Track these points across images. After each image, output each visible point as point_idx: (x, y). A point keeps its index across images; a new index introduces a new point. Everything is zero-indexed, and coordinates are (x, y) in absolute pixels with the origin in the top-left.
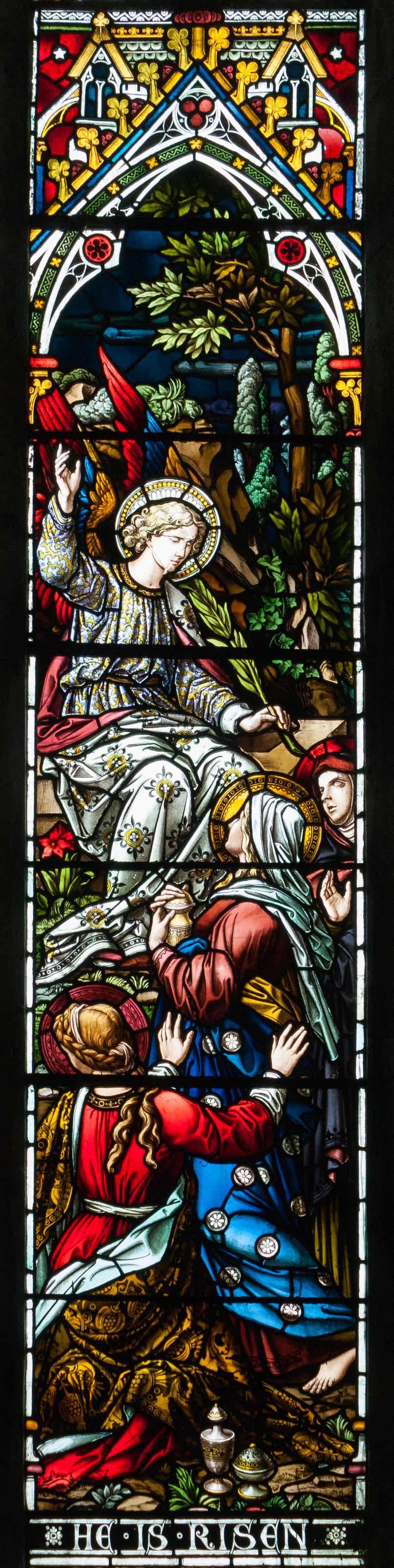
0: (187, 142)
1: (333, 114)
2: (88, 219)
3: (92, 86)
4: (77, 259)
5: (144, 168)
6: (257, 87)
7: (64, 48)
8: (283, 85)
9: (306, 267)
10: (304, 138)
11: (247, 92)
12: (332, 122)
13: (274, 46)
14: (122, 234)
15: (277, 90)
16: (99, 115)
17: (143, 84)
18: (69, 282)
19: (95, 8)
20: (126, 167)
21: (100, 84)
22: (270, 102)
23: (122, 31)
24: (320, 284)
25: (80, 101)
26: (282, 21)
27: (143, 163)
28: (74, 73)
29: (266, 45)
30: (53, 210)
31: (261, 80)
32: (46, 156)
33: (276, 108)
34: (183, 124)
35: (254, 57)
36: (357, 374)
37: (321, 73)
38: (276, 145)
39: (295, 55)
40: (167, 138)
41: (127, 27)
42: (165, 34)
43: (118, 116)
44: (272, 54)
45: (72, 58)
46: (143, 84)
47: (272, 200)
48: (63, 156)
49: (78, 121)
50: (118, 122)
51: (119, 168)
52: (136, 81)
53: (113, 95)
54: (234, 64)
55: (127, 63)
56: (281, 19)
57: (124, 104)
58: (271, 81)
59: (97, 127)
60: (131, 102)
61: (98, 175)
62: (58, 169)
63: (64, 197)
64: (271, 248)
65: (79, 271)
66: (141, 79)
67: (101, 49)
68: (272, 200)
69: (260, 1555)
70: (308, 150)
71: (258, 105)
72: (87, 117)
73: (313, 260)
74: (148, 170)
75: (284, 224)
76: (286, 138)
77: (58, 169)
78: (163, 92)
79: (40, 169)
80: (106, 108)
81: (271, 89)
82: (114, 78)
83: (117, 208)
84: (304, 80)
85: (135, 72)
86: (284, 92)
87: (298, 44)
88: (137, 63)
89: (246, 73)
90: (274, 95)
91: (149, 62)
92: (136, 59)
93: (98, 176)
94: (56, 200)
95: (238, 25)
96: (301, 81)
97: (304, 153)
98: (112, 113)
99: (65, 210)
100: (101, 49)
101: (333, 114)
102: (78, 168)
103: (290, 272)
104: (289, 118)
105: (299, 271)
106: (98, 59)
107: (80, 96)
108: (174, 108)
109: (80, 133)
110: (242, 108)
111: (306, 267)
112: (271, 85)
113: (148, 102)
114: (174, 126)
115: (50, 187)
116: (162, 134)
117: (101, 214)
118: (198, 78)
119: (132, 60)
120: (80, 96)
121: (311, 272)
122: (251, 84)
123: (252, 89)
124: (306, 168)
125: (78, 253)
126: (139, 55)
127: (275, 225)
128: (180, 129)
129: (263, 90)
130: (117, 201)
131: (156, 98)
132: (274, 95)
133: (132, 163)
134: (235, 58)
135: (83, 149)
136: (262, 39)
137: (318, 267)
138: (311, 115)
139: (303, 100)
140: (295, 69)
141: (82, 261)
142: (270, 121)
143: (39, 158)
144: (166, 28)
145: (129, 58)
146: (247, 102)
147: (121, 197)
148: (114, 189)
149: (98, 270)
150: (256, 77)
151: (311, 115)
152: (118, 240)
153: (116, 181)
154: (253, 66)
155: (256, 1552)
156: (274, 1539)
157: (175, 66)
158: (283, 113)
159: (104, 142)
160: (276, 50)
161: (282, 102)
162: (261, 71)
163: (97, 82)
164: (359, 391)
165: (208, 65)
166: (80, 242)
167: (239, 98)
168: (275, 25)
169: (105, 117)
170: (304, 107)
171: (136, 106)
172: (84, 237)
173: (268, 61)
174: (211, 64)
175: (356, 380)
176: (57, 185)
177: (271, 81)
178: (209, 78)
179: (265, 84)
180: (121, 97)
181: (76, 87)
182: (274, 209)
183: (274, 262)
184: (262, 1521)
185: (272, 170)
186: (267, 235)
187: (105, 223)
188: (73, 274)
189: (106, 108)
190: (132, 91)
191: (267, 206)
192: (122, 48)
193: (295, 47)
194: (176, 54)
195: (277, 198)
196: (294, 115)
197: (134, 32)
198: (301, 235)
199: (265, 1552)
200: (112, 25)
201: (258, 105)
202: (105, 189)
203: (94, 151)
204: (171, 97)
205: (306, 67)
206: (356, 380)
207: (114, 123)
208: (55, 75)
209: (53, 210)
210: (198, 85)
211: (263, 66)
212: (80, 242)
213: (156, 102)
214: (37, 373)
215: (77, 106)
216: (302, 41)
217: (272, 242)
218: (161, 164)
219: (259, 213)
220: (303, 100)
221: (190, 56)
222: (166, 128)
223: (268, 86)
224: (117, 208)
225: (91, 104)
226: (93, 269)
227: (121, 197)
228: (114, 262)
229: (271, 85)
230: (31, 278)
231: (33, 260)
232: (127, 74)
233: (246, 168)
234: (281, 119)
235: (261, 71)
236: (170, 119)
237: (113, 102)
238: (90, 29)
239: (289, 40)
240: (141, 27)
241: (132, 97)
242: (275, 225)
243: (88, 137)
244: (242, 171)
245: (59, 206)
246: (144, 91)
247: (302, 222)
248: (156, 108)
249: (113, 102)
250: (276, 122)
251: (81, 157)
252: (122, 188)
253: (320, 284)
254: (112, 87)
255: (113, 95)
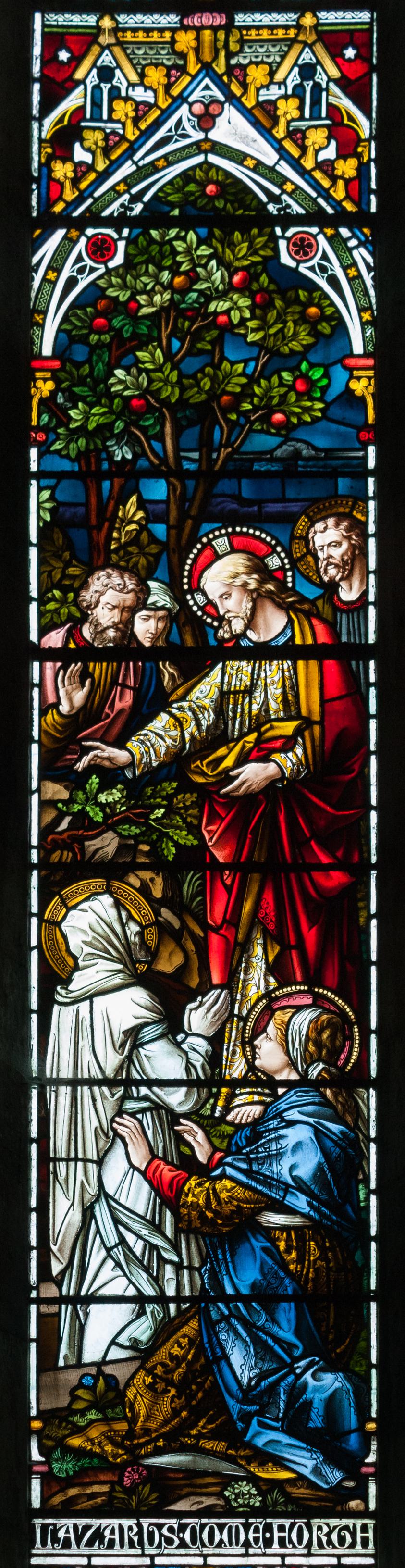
0: (197, 144)
1: (347, 112)
2: (93, 218)
3: (97, 88)
4: (79, 259)
5: (153, 168)
6: (268, 90)
7: (69, 50)
8: (295, 87)
9: (319, 264)
10: (317, 137)
11: (258, 95)
12: (346, 122)
13: (286, 49)
14: (126, 232)
15: (290, 92)
16: (105, 116)
17: (151, 88)
18: (71, 283)
19: (103, 10)
20: (134, 168)
21: (106, 87)
22: (281, 104)
23: (129, 34)
24: (333, 281)
25: (85, 102)
26: (294, 23)
27: (152, 163)
28: (79, 75)
29: (277, 49)
30: (59, 207)
31: (272, 82)
32: (50, 158)
33: (288, 109)
34: (194, 127)
35: (265, 59)
36: (371, 373)
37: (335, 73)
38: (288, 145)
39: (307, 57)
40: (177, 141)
41: (134, 30)
42: (172, 37)
43: (94, 147)
44: (283, 57)
45: (76, 60)
46: (151, 88)
47: (285, 197)
48: (67, 157)
49: (83, 124)
50: (124, 125)
51: (127, 169)
52: (142, 84)
53: (119, 97)
54: (243, 68)
55: (134, 66)
56: (294, 20)
57: (129, 108)
58: (284, 82)
59: (102, 129)
60: (138, 104)
61: (166, 114)
62: (62, 170)
63: (69, 195)
64: (282, 244)
65: (81, 271)
66: (147, 82)
67: (107, 52)
68: (285, 197)
69: (246, 1555)
70: (321, 149)
71: (269, 108)
72: (92, 119)
73: (325, 257)
74: (157, 170)
75: (298, 220)
76: (297, 136)
77: (62, 170)
78: (78, 189)
79: (45, 170)
80: (111, 110)
81: (283, 91)
82: (119, 79)
83: (126, 203)
84: (317, 80)
85: (142, 76)
86: (298, 92)
87: (311, 46)
88: (144, 67)
89: (257, 75)
90: (286, 97)
91: (156, 65)
92: (143, 62)
93: (115, 166)
94: (60, 198)
95: (248, 28)
96: (314, 81)
97: (317, 152)
98: (118, 115)
99: (69, 210)
100: (107, 52)
101: (347, 112)
102: (80, 170)
103: (303, 269)
104: (302, 118)
105: (312, 269)
106: (103, 61)
107: (85, 96)
108: (184, 110)
109: (87, 134)
110: (254, 111)
111: (319, 264)
112: (283, 87)
113: (156, 105)
114: (184, 129)
115: (53, 188)
116: (172, 137)
117: (106, 213)
118: (207, 81)
119: (139, 64)
120: (85, 96)
121: (323, 269)
122: (262, 87)
123: (262, 92)
124: (319, 166)
125: (80, 254)
126: (145, 59)
127: (287, 220)
128: (190, 131)
129: (274, 92)
130: (126, 197)
131: (163, 102)
132: (286, 97)
133: (141, 163)
134: (245, 62)
135: (88, 150)
136: (274, 42)
137: (330, 263)
138: (324, 114)
139: (316, 102)
140: (307, 71)
141: (84, 261)
142: (282, 122)
143: (43, 160)
144: (174, 30)
145: (135, 62)
146: (259, 104)
147: (130, 194)
148: (122, 187)
149: (102, 269)
150: (265, 80)
151: (324, 114)
152: (121, 238)
153: (124, 180)
154: (264, 69)
155: (243, 1551)
156: (259, 1538)
157: (183, 70)
158: (296, 114)
159: (79, 174)
160: (287, 53)
161: (293, 103)
162: (272, 74)
163: (102, 85)
164: (371, 389)
165: (217, 69)
166: (83, 241)
167: (250, 103)
168: (286, 28)
169: (110, 120)
170: (316, 108)
171: (141, 109)
172: (86, 236)
173: (279, 64)
174: (220, 67)
175: (369, 378)
176: (62, 185)
177: (284, 82)
178: (217, 79)
179: (277, 87)
180: (127, 99)
181: (82, 87)
182: (288, 206)
183: (286, 259)
184: (251, 1521)
185: (285, 169)
186: (278, 231)
187: (110, 222)
188: (75, 274)
189: (111, 110)
190: (139, 94)
191: (282, 203)
192: (129, 51)
193: (307, 49)
194: (183, 56)
195: (290, 195)
196: (307, 114)
197: (141, 35)
198: (314, 230)
199: (251, 1551)
200: (115, 30)
201: (269, 108)
202: (113, 188)
203: (129, 123)
204: (86, 194)
205: (319, 68)
206: (369, 378)
207: (120, 126)
208: (60, 77)
209: (59, 207)
210: (207, 88)
211: (274, 68)
212: (83, 241)
213: (164, 106)
214: (38, 375)
215: (82, 108)
216: (314, 43)
217: (283, 237)
218: (170, 164)
219: (272, 208)
220: (316, 102)
221: (199, 60)
222: (176, 130)
223: (280, 88)
224: (126, 203)
225: (97, 104)
226: (96, 269)
227: (130, 194)
228: (118, 260)
229: (283, 87)
230: (33, 279)
231: (35, 260)
232: (134, 78)
233: (259, 167)
234: (293, 120)
235: (272, 74)
236: (179, 122)
237: (119, 105)
238: (94, 31)
239: (300, 42)
240: (148, 31)
241: (139, 99)
242: (287, 220)
243: (93, 138)
244: (254, 170)
245: (158, 112)
246: (150, 93)
247: (316, 217)
248: (163, 111)
249: (119, 105)
250: (288, 123)
251: (88, 158)
252: (130, 187)
253: (333, 281)
254: (118, 89)
255: (119, 97)
